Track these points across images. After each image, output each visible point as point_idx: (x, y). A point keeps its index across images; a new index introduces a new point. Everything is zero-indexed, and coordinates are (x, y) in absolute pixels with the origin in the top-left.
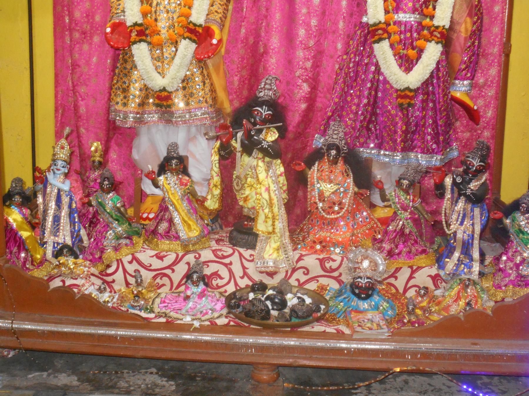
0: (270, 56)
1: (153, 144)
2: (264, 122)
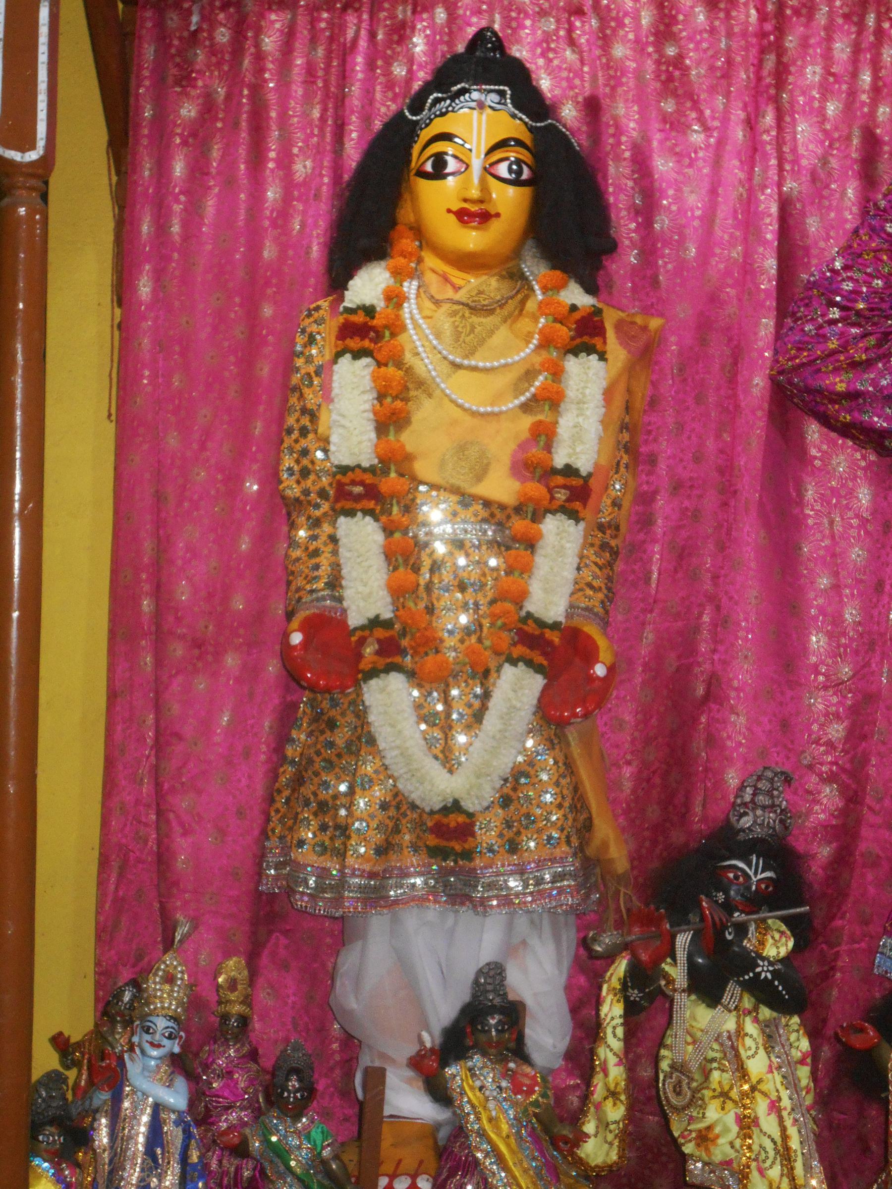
1: (404, 967)
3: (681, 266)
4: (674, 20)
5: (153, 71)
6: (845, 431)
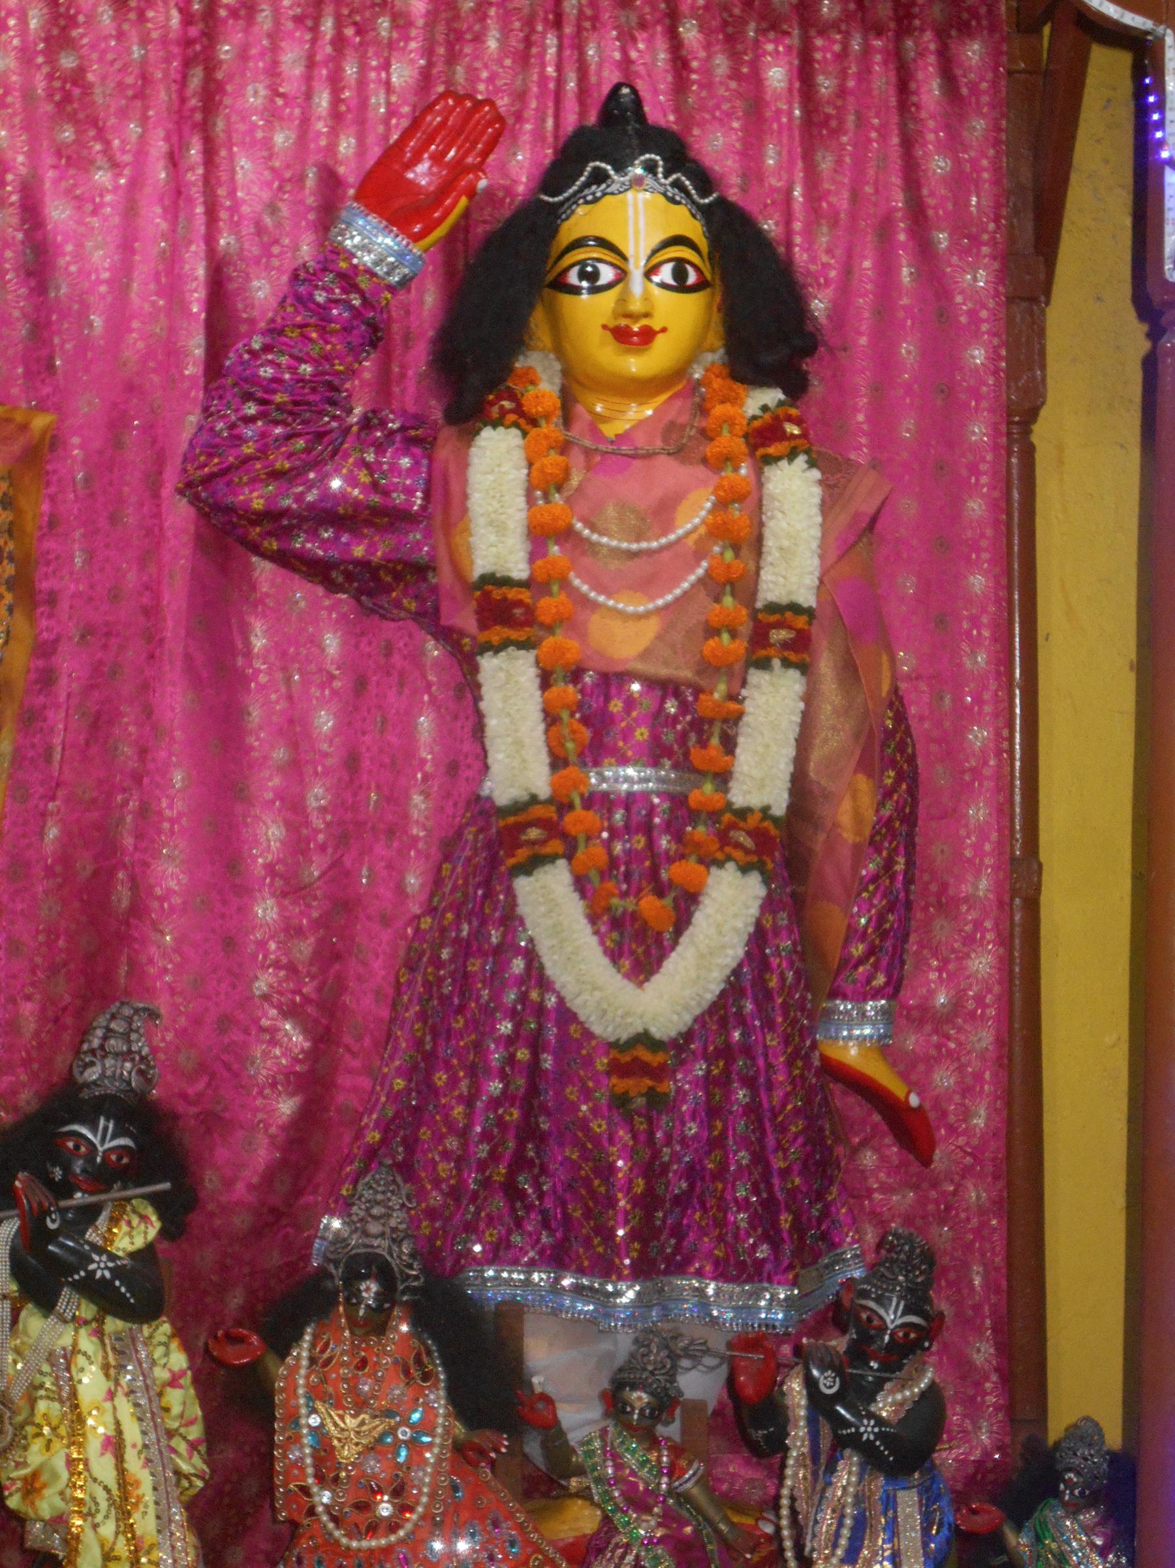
0: (153, 923)
2: (106, 1176)
3: (83, 346)
4: (72, 22)
6: (285, 560)
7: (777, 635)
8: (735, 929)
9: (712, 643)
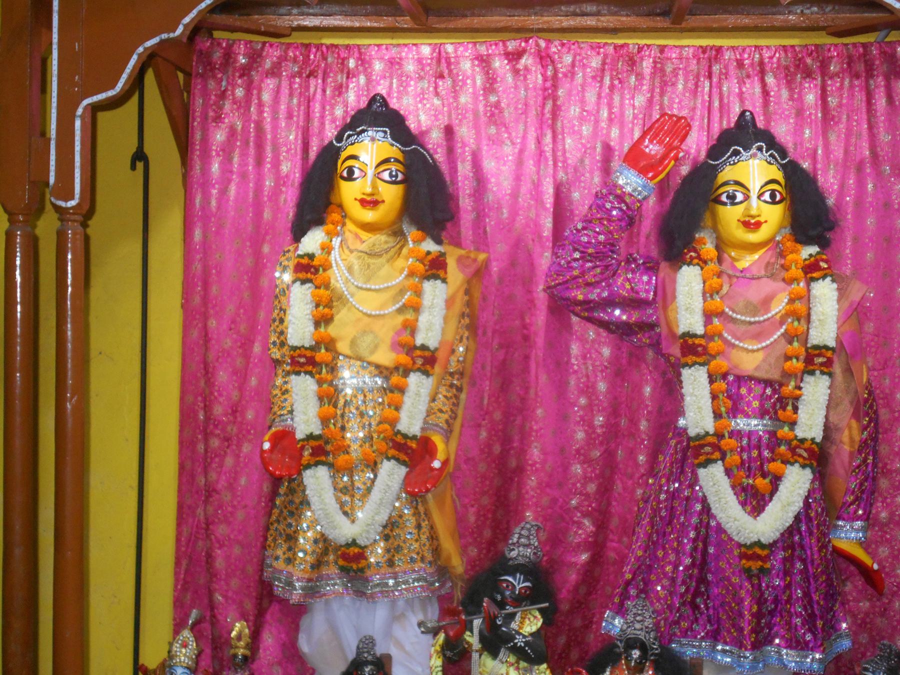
2: (520, 600)
3: (499, 222)
4: (494, 81)
5: (201, 113)
6: (589, 320)
7: (816, 359)
8: (799, 494)
9: (789, 363)
